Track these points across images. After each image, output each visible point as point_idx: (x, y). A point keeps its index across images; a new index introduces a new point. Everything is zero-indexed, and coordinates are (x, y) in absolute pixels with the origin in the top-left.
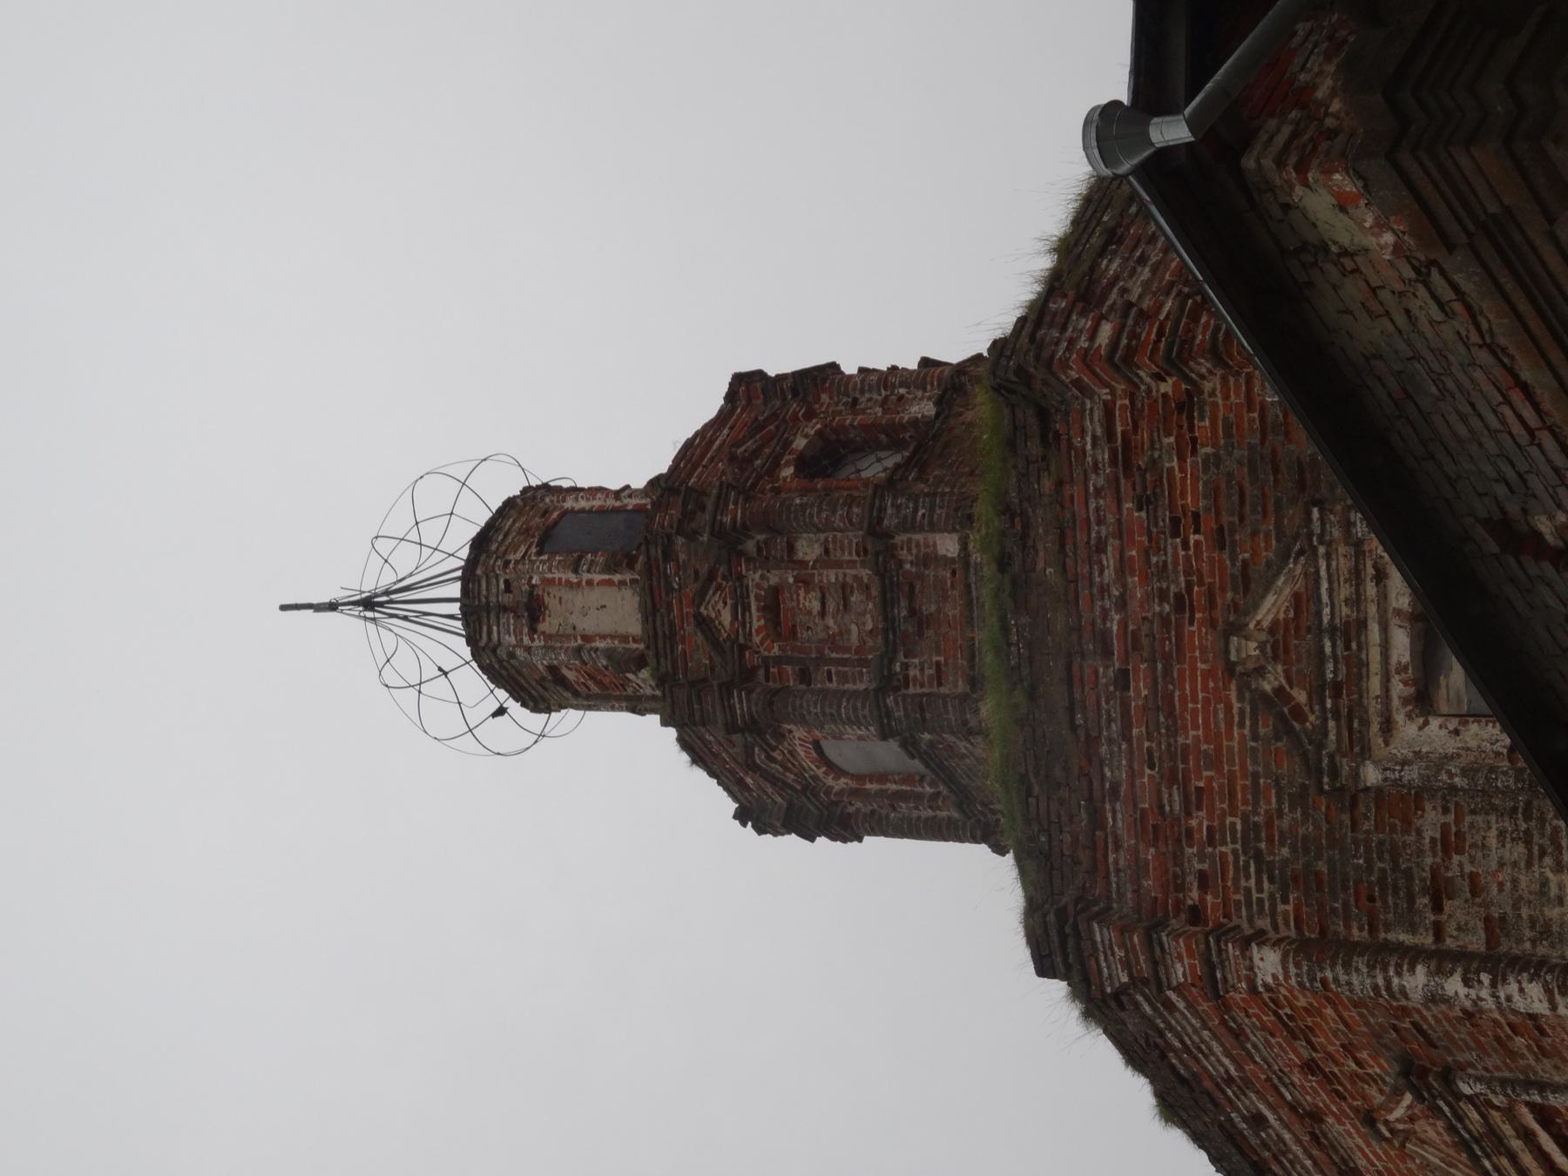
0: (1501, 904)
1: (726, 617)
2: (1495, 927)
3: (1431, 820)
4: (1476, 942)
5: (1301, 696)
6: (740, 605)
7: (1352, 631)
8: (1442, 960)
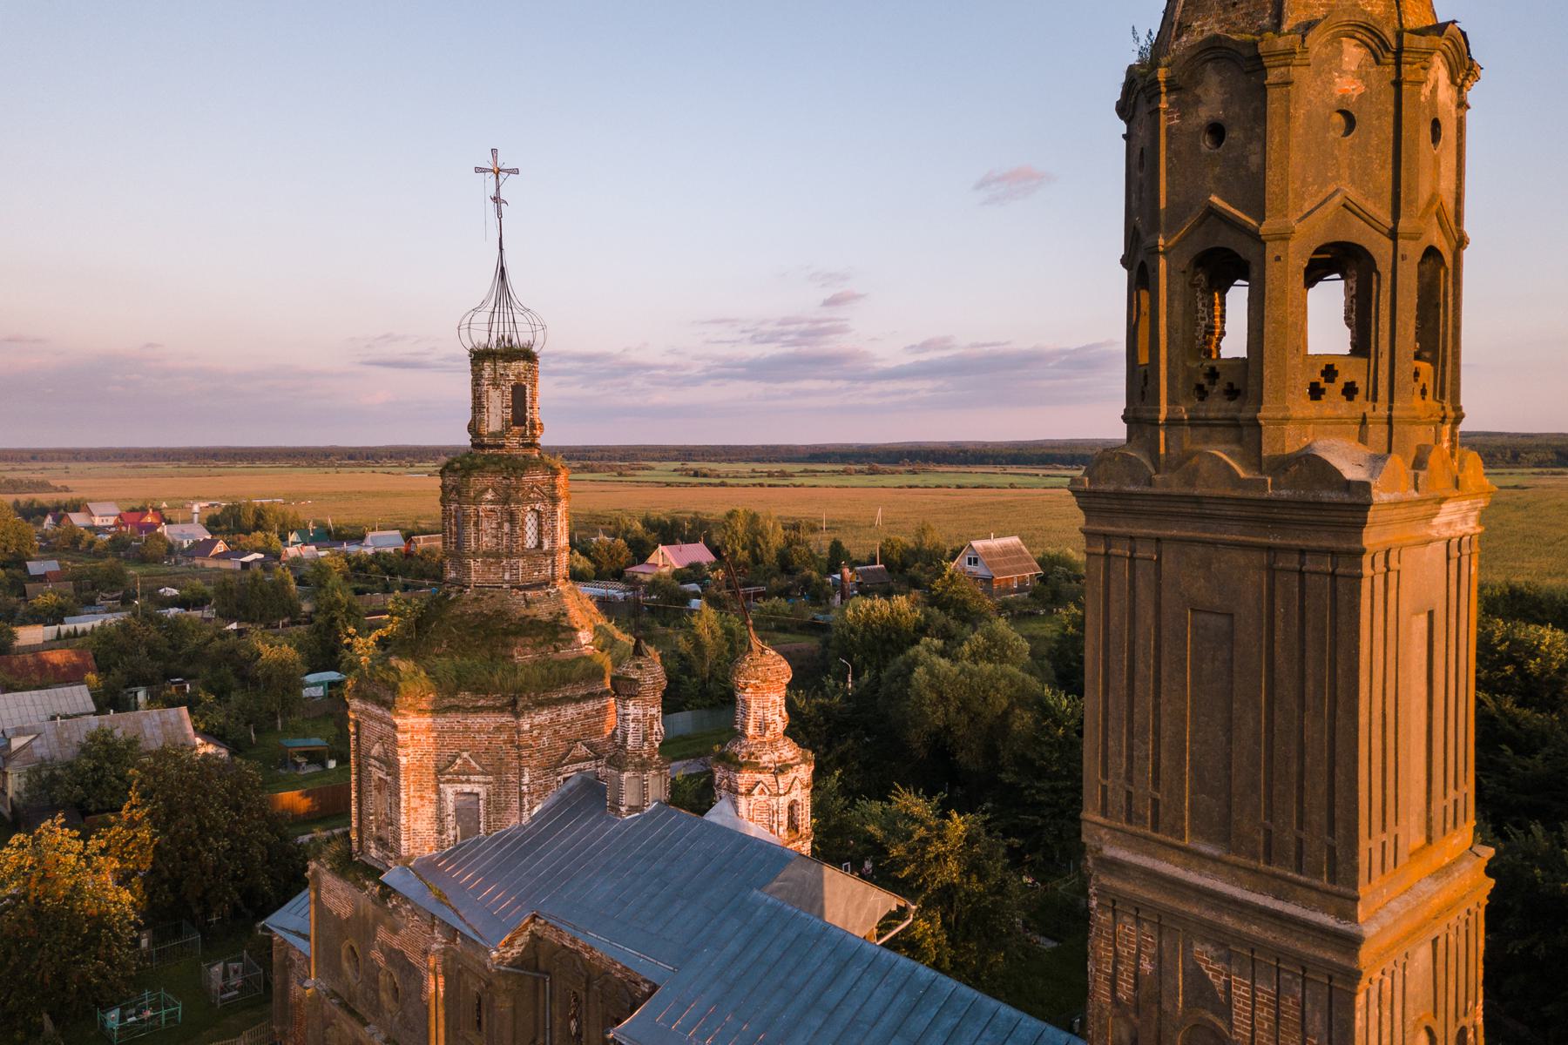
0: (420, 811)
2: (416, 809)
5: (456, 768)
7: (468, 781)
8: (408, 801)
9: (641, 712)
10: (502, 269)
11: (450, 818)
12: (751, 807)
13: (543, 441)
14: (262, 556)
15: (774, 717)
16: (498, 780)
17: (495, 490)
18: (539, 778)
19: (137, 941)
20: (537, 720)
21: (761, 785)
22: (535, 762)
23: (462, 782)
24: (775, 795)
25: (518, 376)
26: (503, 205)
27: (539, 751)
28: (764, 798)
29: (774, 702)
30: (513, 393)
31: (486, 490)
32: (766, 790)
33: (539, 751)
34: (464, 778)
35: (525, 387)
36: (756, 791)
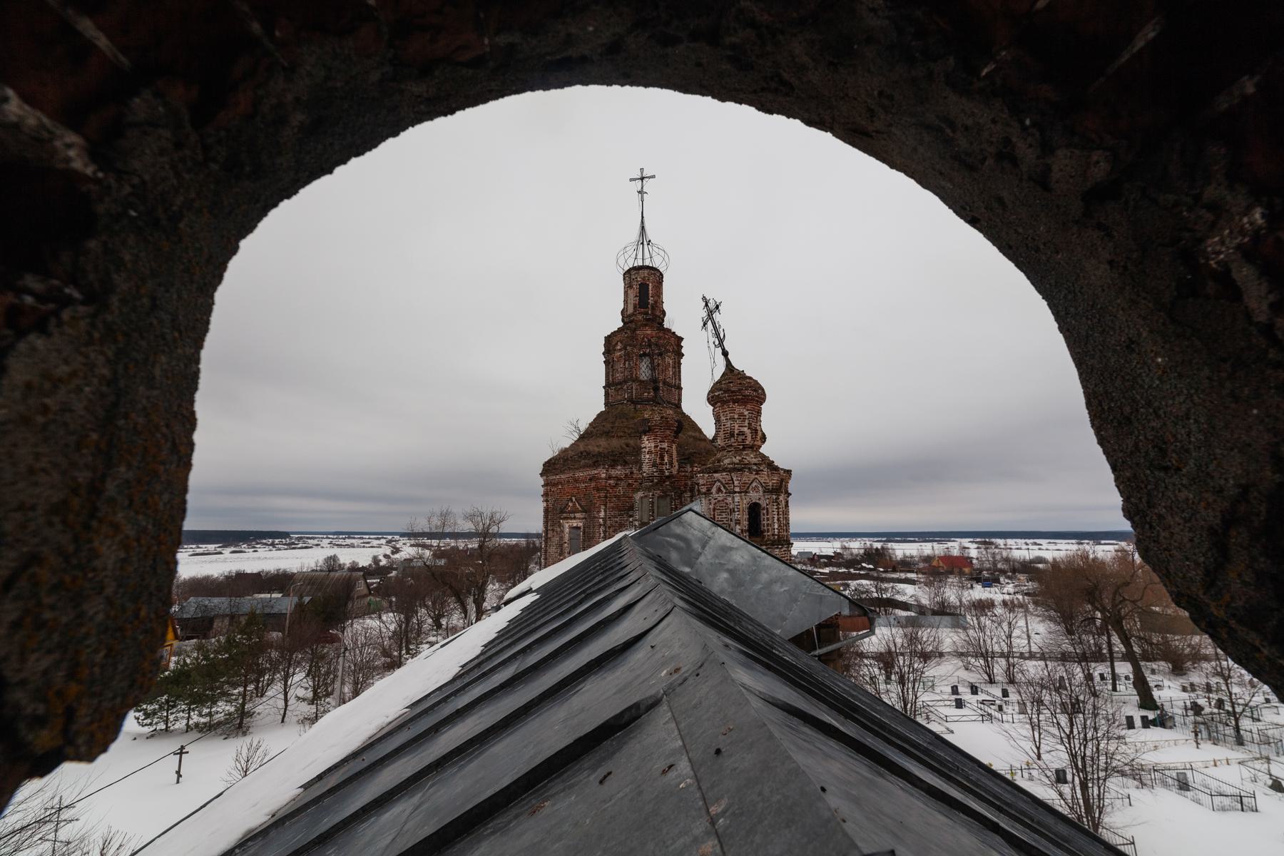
1: (619, 347)
3: (559, 529)
4: (549, 536)
6: (620, 350)
9: (653, 445)
10: (643, 228)
11: (566, 545)
12: (711, 507)
13: (764, 450)
14: (826, 561)
15: (742, 429)
16: (589, 516)
17: (621, 342)
18: (615, 517)
19: (930, 580)
20: (613, 472)
21: (718, 484)
22: (612, 504)
23: (571, 519)
24: (730, 493)
25: (643, 279)
26: (645, 195)
27: (615, 496)
28: (721, 496)
29: (741, 415)
30: (640, 289)
31: (617, 344)
32: (722, 488)
33: (615, 496)
34: (572, 515)
35: (648, 285)
36: (714, 490)
